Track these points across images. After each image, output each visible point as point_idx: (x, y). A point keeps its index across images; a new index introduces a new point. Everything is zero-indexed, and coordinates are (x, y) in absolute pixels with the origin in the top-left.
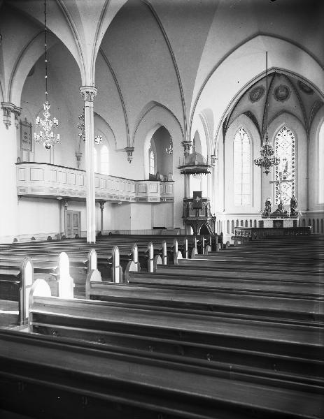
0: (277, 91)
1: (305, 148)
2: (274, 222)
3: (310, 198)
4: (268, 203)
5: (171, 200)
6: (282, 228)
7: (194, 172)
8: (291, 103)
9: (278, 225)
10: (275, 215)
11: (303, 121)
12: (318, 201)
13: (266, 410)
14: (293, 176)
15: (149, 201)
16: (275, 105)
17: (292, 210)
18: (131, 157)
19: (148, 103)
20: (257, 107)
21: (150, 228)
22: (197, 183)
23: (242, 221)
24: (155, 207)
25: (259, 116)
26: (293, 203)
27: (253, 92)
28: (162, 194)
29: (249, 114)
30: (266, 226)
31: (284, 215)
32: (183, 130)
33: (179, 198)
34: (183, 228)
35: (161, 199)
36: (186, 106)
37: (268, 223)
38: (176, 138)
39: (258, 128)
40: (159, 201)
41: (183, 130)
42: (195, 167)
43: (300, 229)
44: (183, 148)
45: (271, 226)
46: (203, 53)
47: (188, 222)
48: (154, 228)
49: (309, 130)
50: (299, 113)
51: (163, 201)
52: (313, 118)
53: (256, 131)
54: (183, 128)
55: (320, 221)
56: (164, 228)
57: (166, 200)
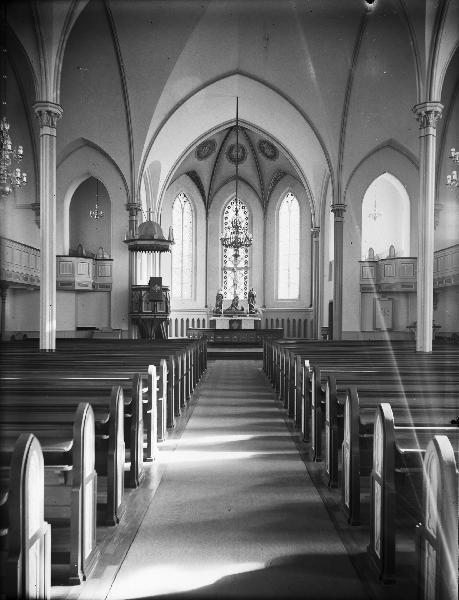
0: (231, 149)
1: (261, 227)
2: (231, 322)
3: (268, 292)
4: (219, 298)
5: (106, 288)
6: (239, 330)
7: (143, 249)
8: (247, 168)
9: (235, 326)
10: (228, 313)
11: (260, 195)
12: (277, 296)
13: (235, 577)
14: (246, 263)
15: (77, 287)
16: (228, 167)
17: (251, 307)
18: (339, 219)
19: (77, 140)
20: (204, 168)
21: (74, 329)
22: (146, 268)
23: (198, 320)
24: (80, 297)
25: (206, 177)
26: (251, 296)
27: (203, 149)
28: (95, 277)
29: (194, 176)
30: (219, 326)
31: (241, 313)
32: (335, 171)
33: (120, 284)
34: (125, 327)
35: (93, 286)
36: (136, 152)
37: (222, 323)
38: (118, 199)
39: (203, 195)
40: (90, 288)
41: (335, 171)
42: (153, 242)
43: (352, 345)
44: (34, 213)
45: (226, 326)
46: (173, 72)
47: (135, 320)
48: (79, 329)
49: (267, 206)
50: (255, 183)
51: (96, 288)
52: (272, 191)
53: (201, 200)
54: (129, 184)
55: (291, 322)
56: (94, 328)
57: (102, 288)
